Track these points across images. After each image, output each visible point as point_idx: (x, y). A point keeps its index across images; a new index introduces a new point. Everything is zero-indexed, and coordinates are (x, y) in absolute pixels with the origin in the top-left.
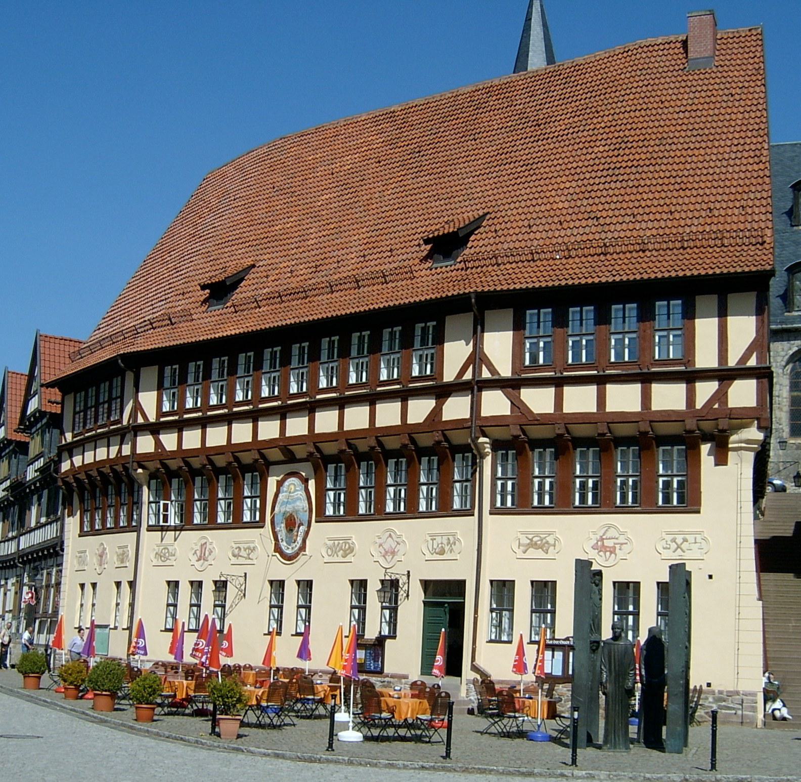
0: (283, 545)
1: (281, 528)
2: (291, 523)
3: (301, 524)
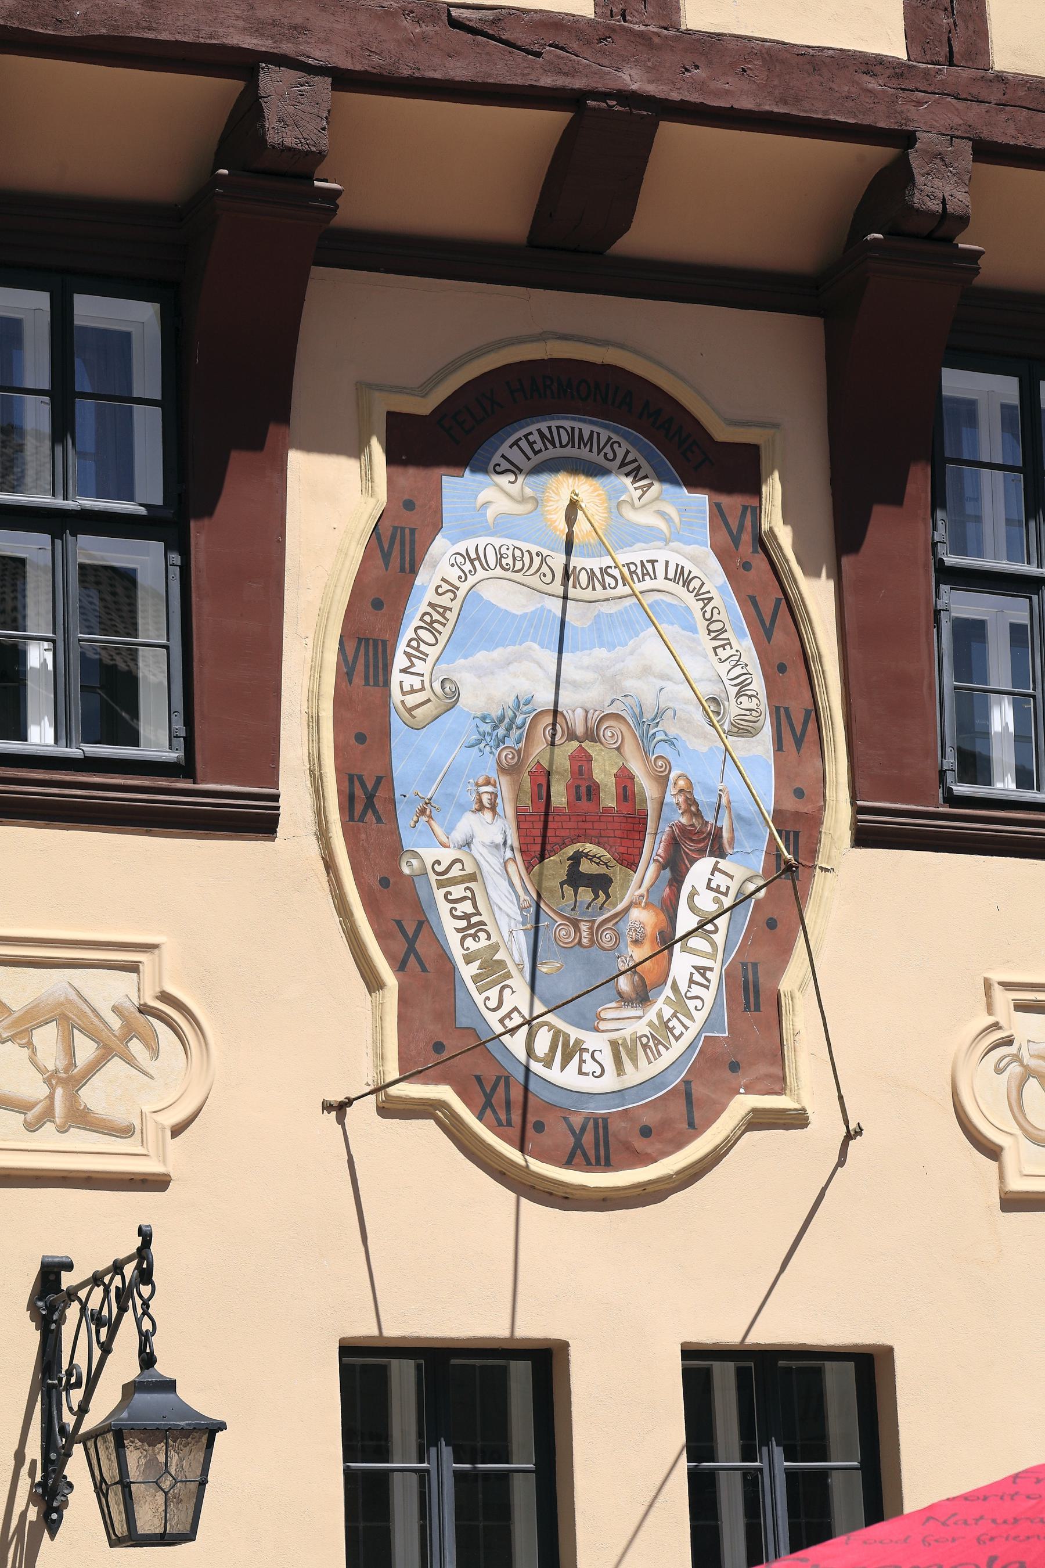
0: (500, 1006)
1: (467, 847)
2: (581, 824)
3: (699, 838)
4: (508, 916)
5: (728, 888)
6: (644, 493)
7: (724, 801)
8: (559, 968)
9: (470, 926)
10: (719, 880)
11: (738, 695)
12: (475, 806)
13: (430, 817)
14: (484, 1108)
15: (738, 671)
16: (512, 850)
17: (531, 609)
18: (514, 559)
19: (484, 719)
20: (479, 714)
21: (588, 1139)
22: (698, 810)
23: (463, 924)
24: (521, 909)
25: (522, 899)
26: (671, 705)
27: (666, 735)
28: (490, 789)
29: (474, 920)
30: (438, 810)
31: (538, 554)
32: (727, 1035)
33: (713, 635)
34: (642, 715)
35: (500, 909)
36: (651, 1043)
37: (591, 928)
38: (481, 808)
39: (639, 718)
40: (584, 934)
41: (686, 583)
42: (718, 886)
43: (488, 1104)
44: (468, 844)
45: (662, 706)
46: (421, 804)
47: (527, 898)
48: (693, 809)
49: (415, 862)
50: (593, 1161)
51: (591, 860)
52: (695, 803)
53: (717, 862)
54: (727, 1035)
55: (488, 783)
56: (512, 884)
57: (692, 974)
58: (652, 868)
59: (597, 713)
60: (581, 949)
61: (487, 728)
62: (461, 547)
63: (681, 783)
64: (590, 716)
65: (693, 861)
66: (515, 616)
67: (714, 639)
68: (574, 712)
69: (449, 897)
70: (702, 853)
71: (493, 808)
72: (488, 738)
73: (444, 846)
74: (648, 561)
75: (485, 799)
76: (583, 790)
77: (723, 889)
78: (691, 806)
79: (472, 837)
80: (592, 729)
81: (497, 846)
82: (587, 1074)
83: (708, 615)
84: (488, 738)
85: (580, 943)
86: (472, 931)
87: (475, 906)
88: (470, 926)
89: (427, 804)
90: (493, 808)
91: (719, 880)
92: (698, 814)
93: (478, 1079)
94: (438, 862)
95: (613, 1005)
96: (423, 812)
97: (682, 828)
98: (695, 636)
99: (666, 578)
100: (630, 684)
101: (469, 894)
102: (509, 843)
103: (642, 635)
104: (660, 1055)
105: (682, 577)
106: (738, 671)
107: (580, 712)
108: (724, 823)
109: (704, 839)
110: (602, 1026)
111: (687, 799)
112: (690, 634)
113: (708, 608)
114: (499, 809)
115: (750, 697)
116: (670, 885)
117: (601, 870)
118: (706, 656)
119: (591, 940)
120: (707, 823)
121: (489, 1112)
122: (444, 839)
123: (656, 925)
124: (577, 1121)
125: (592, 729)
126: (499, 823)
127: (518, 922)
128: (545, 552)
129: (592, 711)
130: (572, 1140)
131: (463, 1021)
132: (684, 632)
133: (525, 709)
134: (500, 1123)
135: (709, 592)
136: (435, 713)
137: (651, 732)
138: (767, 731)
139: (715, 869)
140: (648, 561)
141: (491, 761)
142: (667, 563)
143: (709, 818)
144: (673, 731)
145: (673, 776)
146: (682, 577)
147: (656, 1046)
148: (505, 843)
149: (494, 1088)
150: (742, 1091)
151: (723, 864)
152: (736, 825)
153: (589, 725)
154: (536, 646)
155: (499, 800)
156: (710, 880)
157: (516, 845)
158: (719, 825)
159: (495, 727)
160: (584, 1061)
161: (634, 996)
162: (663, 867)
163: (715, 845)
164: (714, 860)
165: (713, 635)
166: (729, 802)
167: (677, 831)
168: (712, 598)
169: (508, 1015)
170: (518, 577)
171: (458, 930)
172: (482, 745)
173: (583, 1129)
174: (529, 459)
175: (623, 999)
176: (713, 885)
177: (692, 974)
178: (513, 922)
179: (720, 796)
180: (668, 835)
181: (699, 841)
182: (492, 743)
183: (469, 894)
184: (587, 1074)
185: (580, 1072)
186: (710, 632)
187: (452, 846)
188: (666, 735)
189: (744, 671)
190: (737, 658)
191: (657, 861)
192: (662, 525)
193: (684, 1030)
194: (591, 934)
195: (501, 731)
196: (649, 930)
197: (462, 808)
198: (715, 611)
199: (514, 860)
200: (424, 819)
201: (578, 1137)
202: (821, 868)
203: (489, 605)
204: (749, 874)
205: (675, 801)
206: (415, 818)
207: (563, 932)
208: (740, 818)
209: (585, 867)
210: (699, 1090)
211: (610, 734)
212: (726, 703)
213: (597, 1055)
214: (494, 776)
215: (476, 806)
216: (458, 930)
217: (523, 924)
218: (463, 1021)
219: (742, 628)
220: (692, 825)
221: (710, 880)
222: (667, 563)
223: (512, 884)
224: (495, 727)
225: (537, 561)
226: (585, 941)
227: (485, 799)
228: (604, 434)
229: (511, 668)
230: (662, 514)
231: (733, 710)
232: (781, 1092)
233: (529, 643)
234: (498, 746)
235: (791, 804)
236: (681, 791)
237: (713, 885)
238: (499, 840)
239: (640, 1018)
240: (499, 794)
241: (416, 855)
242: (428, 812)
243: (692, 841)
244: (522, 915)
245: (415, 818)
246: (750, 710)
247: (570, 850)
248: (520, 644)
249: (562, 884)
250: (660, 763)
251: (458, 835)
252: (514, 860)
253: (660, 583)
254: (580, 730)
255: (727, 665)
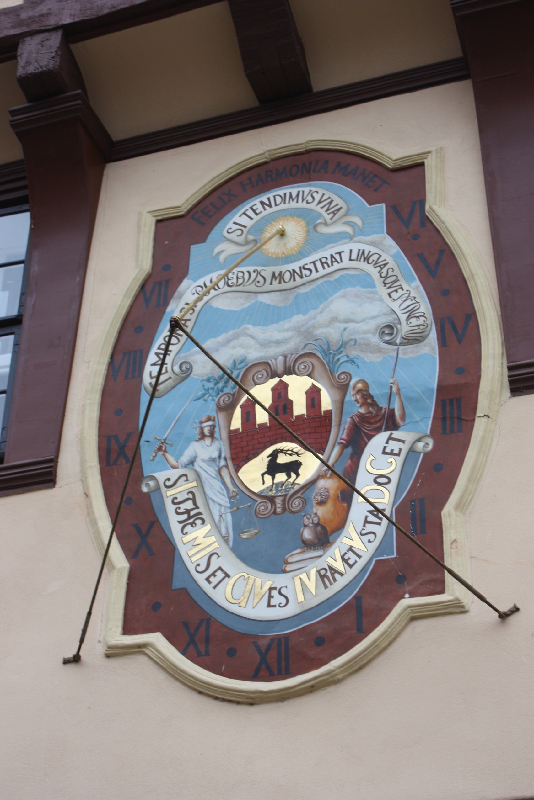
4: (220, 505)
5: (400, 450)
6: (335, 214)
7: (394, 390)
8: (257, 534)
9: (190, 517)
10: (394, 446)
11: (408, 318)
12: (198, 437)
13: (165, 451)
14: (188, 645)
15: (409, 302)
16: (225, 459)
17: (247, 305)
18: (238, 278)
19: (208, 380)
20: (205, 378)
21: (273, 654)
22: (373, 401)
23: (185, 516)
24: (230, 498)
25: (231, 491)
26: (353, 337)
27: (348, 357)
28: (210, 423)
29: (192, 513)
30: (171, 445)
31: (254, 271)
32: (395, 555)
33: (388, 286)
34: (329, 349)
35: (214, 501)
36: (329, 574)
37: (284, 501)
38: (203, 436)
39: (326, 353)
40: (278, 505)
41: (367, 259)
42: (392, 450)
43: (192, 641)
44: (192, 463)
45: (345, 339)
46: (158, 444)
47: (235, 490)
48: (369, 401)
49: (152, 483)
50: (275, 672)
51: (285, 453)
52: (371, 397)
53: (391, 434)
54: (395, 555)
55: (209, 419)
56: (224, 483)
57: (367, 517)
58: (337, 449)
59: (293, 356)
60: (276, 516)
61: (211, 385)
62: (200, 282)
63: (360, 386)
64: (288, 359)
65: (370, 437)
66: (236, 311)
67: (390, 287)
68: (276, 359)
69: (176, 501)
70: (378, 430)
71: (212, 435)
72: (211, 391)
73: (174, 467)
74: (336, 253)
75: (206, 431)
76: (280, 408)
77: (396, 451)
78: (366, 396)
79: (195, 457)
80: (290, 367)
81: (213, 460)
82: (274, 606)
83: (383, 275)
84: (211, 391)
85: (275, 513)
86: (191, 521)
87: (195, 503)
88: (190, 517)
89: (162, 443)
90: (212, 435)
91: (394, 446)
92: (374, 404)
93: (186, 625)
94: (169, 479)
95: (298, 551)
96: (160, 449)
97: (361, 417)
98: (374, 290)
99: (350, 260)
100: (319, 332)
101: (190, 496)
102: (223, 455)
103: (330, 299)
104: (335, 580)
105: (364, 257)
106: (409, 302)
107: (281, 359)
108: (396, 406)
109: (380, 420)
110: (288, 568)
111: (363, 396)
112: (370, 289)
113: (384, 271)
114: (217, 435)
115: (418, 317)
116: (351, 458)
117: (294, 458)
118: (381, 300)
119: (284, 510)
120: (381, 408)
121: (191, 647)
122: (174, 462)
123: (338, 488)
124: (263, 643)
125: (290, 367)
126: (216, 444)
127: (227, 507)
128: (259, 268)
129: (289, 356)
130: (258, 658)
131: (177, 584)
132: (364, 290)
133: (240, 366)
134: (199, 654)
135: (337, 205)
136: (173, 384)
137: (336, 358)
138: (433, 336)
139: (390, 438)
140: (336, 253)
141: (212, 406)
142: (351, 251)
143: (383, 404)
144: (353, 353)
145: (352, 383)
146: (364, 257)
147: (332, 575)
148: (220, 457)
149: (197, 629)
150: (407, 596)
151: (396, 434)
152: (406, 404)
153: (287, 365)
154: (250, 326)
155: (217, 429)
156: (385, 448)
157: (228, 456)
158: (391, 407)
159: (217, 383)
160: (273, 597)
161: (316, 541)
162: (344, 446)
163: (391, 423)
164: (388, 433)
165: (388, 286)
166: (398, 389)
167: (356, 419)
168: (387, 263)
169: (214, 574)
170: (240, 288)
171: (180, 522)
172: (206, 397)
173: (269, 648)
174: (251, 219)
175: (308, 545)
176: (388, 450)
177: (367, 517)
178: (223, 508)
179: (391, 387)
180: (350, 424)
181: (376, 423)
182: (214, 394)
183: (190, 496)
184: (274, 606)
185: (269, 605)
186: (385, 284)
187: (180, 466)
188: (348, 357)
189: (414, 301)
190: (407, 295)
191: (341, 443)
192: (348, 230)
193: (357, 559)
194: (284, 504)
195: (221, 385)
196: (332, 492)
197: (189, 441)
198: (390, 271)
199: (227, 466)
200: (161, 453)
201: (264, 655)
202: (398, 350)
203: (218, 309)
204: (418, 436)
205: (353, 398)
206: (154, 454)
207: (263, 508)
208: (410, 399)
209: (282, 459)
210: (367, 602)
211: (303, 367)
212: (399, 326)
213: (283, 591)
214: (213, 414)
215: (199, 437)
216: (180, 522)
217: (231, 508)
218: (177, 584)
219: (413, 276)
220: (370, 412)
221: (385, 448)
222: (351, 251)
223: (224, 483)
224: (216, 384)
225: (253, 275)
226: (279, 510)
227: (206, 431)
228: (307, 190)
229: (231, 344)
230: (348, 223)
231: (404, 329)
232: (442, 592)
233: (246, 326)
234: (218, 394)
235: (453, 379)
236: (359, 391)
237: (388, 450)
238: (215, 454)
239: (320, 556)
240: (217, 425)
241: (153, 478)
242: (163, 448)
243: (370, 423)
244: (231, 502)
245: (154, 454)
246: (418, 326)
247: (269, 450)
248: (238, 328)
249: (263, 475)
250: (342, 377)
251: (185, 459)
252: (227, 466)
253: (346, 263)
254: (280, 369)
255: (399, 301)
